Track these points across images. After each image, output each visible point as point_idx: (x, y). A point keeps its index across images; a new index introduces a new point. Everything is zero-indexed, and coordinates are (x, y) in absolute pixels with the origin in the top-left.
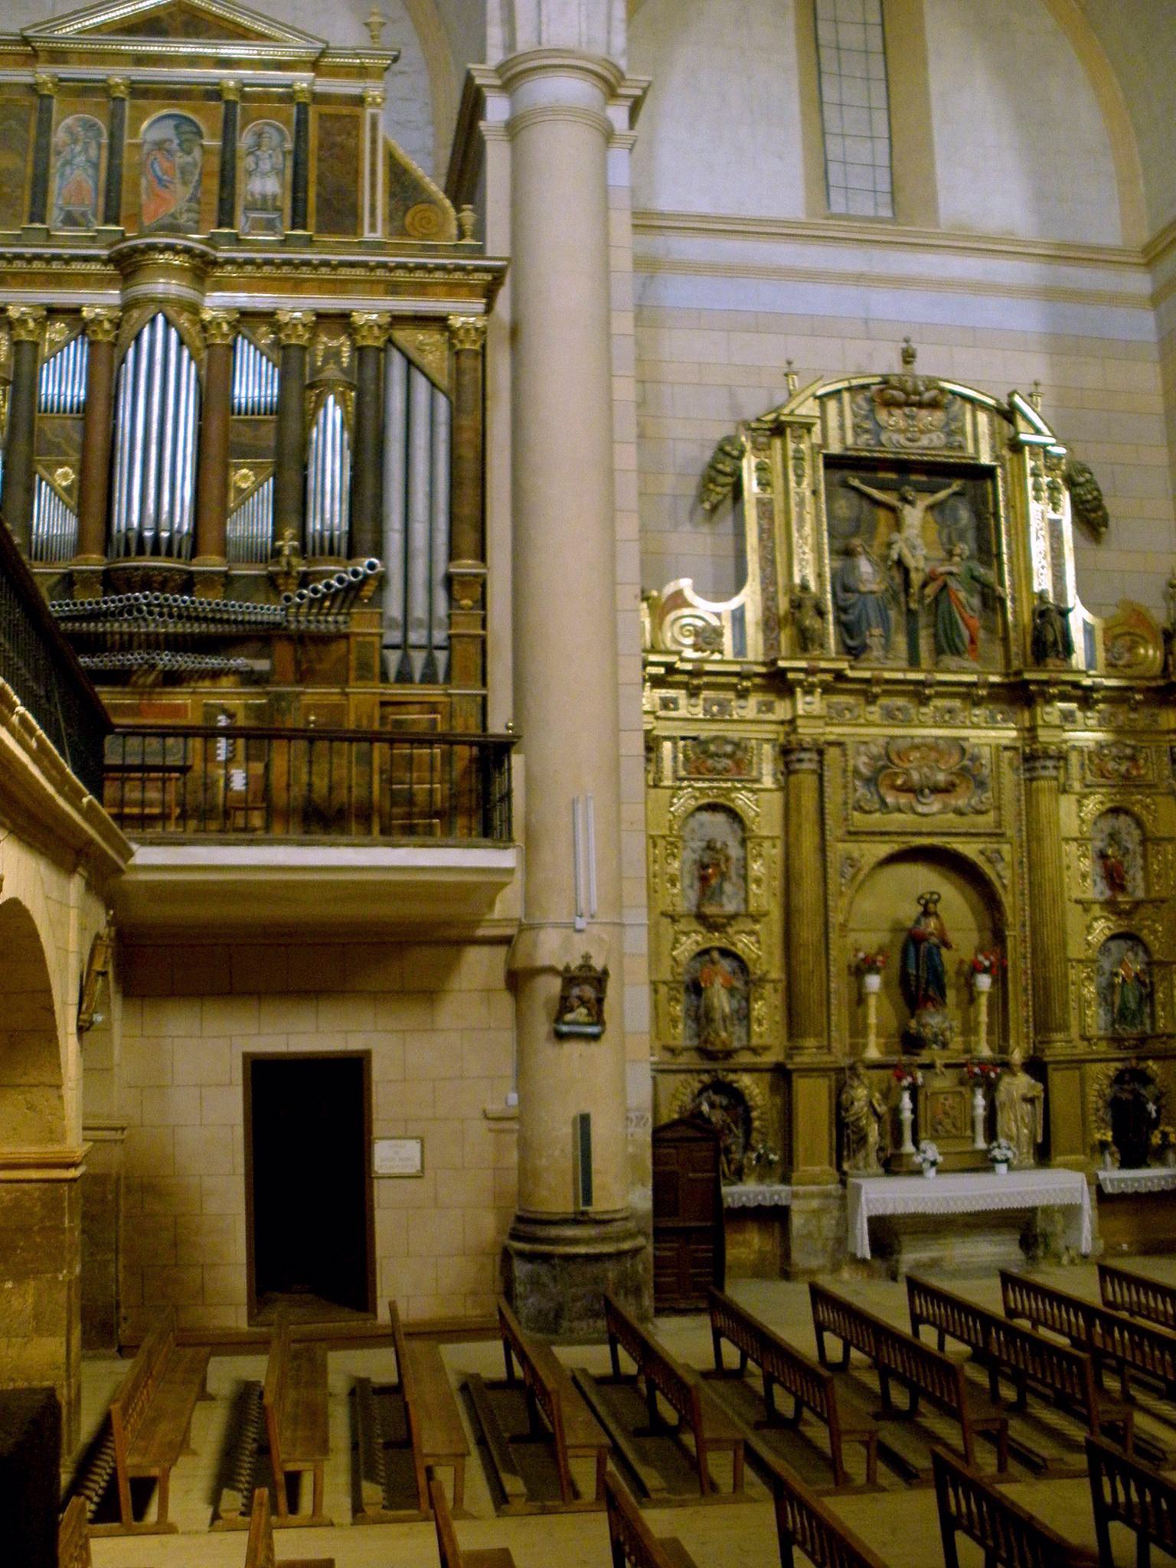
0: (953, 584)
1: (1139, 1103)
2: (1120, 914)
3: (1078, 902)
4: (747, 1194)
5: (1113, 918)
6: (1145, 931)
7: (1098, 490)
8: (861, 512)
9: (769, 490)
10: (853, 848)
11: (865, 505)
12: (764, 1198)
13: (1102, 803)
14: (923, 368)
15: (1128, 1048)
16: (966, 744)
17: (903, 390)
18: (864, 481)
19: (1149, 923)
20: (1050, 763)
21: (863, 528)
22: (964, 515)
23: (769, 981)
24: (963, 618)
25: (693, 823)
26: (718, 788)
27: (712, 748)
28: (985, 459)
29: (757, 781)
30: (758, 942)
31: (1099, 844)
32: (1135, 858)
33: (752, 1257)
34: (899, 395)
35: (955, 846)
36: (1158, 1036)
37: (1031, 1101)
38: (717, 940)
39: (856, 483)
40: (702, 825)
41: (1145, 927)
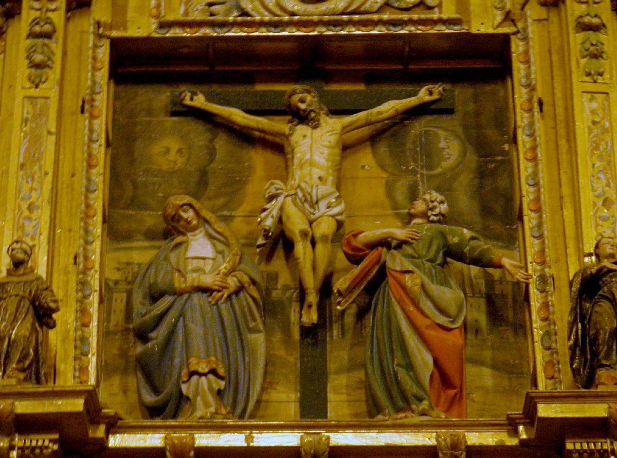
0: (396, 261)
11: (222, 143)
18: (209, 99)
21: (212, 188)
39: (200, 101)
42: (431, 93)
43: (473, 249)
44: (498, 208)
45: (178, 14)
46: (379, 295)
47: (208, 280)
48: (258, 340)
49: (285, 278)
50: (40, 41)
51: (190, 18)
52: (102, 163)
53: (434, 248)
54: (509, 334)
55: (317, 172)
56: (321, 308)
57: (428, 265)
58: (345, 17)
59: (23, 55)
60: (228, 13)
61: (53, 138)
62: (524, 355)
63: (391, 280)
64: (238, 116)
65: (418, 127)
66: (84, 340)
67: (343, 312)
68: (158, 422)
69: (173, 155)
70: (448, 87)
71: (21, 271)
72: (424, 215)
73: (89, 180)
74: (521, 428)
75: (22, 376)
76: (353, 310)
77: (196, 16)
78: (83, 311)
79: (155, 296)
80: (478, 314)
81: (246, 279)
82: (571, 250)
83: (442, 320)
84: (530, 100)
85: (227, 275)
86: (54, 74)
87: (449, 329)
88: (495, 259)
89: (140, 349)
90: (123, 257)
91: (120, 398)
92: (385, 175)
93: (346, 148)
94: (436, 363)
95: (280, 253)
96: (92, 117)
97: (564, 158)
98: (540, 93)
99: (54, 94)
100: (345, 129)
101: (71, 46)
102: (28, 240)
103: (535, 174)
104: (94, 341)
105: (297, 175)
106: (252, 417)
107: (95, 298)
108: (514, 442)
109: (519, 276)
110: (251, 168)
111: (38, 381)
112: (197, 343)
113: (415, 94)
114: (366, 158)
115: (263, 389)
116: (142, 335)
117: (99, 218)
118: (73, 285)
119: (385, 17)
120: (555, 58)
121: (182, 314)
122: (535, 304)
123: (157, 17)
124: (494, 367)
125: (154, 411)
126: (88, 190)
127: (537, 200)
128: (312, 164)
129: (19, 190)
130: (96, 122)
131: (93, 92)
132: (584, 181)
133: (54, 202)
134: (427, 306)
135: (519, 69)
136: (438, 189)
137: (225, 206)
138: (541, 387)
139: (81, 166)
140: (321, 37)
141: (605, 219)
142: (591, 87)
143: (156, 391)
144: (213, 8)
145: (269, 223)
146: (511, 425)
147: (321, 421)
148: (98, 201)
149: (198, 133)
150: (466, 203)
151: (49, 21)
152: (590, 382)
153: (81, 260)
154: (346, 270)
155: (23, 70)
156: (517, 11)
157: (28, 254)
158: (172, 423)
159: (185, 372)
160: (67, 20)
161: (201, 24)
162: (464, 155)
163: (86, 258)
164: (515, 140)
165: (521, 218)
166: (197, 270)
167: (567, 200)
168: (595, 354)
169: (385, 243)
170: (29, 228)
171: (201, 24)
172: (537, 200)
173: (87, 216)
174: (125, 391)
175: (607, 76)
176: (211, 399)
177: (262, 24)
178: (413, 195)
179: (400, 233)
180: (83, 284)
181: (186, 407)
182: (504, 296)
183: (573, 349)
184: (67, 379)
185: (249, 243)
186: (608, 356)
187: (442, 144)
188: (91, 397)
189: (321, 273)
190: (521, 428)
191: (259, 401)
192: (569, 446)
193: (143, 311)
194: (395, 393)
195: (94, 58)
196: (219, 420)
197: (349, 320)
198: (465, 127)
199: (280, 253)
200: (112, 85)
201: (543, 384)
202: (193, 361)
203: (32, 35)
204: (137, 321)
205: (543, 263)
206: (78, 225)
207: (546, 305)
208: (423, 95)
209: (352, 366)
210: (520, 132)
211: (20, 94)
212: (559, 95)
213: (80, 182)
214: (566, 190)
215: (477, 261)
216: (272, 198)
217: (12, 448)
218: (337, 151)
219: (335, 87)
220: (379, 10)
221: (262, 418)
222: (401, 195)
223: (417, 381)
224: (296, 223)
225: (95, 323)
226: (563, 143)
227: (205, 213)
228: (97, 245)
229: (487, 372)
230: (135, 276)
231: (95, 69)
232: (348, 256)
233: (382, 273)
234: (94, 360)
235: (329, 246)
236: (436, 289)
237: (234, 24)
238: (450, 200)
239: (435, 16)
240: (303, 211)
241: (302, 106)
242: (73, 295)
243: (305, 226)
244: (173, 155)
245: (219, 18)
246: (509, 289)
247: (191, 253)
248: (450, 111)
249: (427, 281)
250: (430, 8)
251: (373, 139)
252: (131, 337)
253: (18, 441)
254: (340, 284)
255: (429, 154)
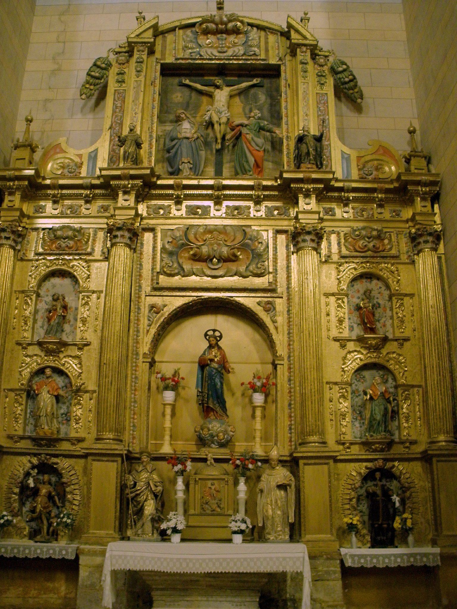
0: (244, 131)
1: (387, 494)
2: (369, 348)
3: (336, 340)
4: (18, 547)
5: (365, 352)
6: (392, 362)
7: (352, 75)
8: (191, 97)
9: (124, 85)
10: (158, 301)
11: (194, 94)
12: (6, 552)
13: (355, 269)
14: (229, 9)
15: (375, 451)
16: (247, 230)
17: (213, 22)
18: (190, 81)
19: (395, 355)
20: (308, 238)
21: (190, 108)
22: (262, 97)
23: (87, 392)
24: (250, 151)
25: (48, 284)
26: (62, 259)
27: (59, 233)
28: (273, 61)
29: (89, 254)
30: (80, 364)
31: (356, 301)
32: (385, 311)
33: (60, 601)
34: (212, 26)
35: (237, 299)
36: (402, 443)
37: (282, 487)
38: (51, 361)
39: (187, 82)
40: (54, 286)
41: (391, 359)
42: (257, 81)
43: (268, 127)
44: (276, 115)
45: (181, 56)
46: (239, 140)
47: (188, 135)
48: (203, 153)
49: (211, 135)
50: (139, 64)
51: (185, 57)
52: (157, 100)
53: (256, 127)
54: (277, 153)
55: (222, 104)
56: (222, 144)
57: (254, 132)
58: (231, 57)
59: (134, 68)
60: (196, 56)
61: (142, 93)
62: (281, 159)
63: (243, 136)
64: (199, 86)
65: (253, 91)
66: (151, 153)
67: (229, 145)
68: (172, 177)
69: (179, 98)
70: (262, 79)
71: (132, 132)
72: (253, 117)
73: (153, 105)
74: (279, 180)
75: (132, 163)
76: (232, 145)
77: (187, 56)
78: (151, 144)
79: (172, 140)
80: (269, 147)
81: (199, 135)
82: (296, 127)
83: (258, 148)
84: (286, 84)
85: (194, 134)
86: (143, 74)
87: (259, 151)
88: (274, 131)
89: (167, 155)
90: (164, 128)
91: (162, 170)
92: (242, 105)
93: (231, 97)
94: (255, 161)
95: (210, 127)
96: (155, 86)
97: (295, 102)
98: (289, 82)
99: (143, 80)
100: (231, 91)
101: (149, 66)
102: (134, 123)
103: (286, 106)
104: (154, 153)
105: (216, 105)
106: (201, 175)
107: (154, 140)
108: (276, 184)
109: (281, 136)
110: (202, 102)
111: (137, 165)
112: (184, 154)
113: (252, 81)
114: (237, 100)
115: (204, 167)
116: (168, 151)
117: (156, 117)
118: (148, 136)
119: (244, 58)
120: (294, 72)
121: (180, 145)
122: (285, 144)
123: (175, 57)
124: (272, 162)
125: (171, 174)
126: (153, 108)
127: (287, 113)
128: (220, 101)
129: (132, 109)
130: (156, 74)
131: (155, 79)
132: (300, 108)
133: (143, 111)
134: (253, 144)
135: (283, 74)
136: (258, 110)
137: (194, 113)
138: (285, 169)
139: (151, 101)
140: (224, 64)
141: (305, 120)
142: (303, 81)
143: (172, 167)
144: (192, 54)
145: (207, 118)
146: (276, 179)
147: (220, 177)
148: (156, 112)
149: (186, 91)
150: (266, 113)
151: (142, 58)
152: (299, 167)
153: (151, 129)
154: (230, 133)
155: (134, 73)
156: (283, 57)
157: (135, 127)
158: (176, 177)
159: (180, 162)
160: (148, 57)
161: (188, 59)
162: (266, 99)
163: (152, 128)
164: (281, 96)
165: (282, 118)
166: (185, 132)
167: (296, 114)
168: (301, 159)
169: (242, 125)
170: (135, 119)
171: (188, 59)
172: (287, 113)
173: (152, 116)
174: (163, 167)
175: (308, 78)
176: (188, 170)
177: (206, 59)
178: (251, 111)
179: (246, 122)
180: (151, 136)
181: (181, 172)
182: (276, 141)
183: (295, 157)
184: (146, 164)
185: (201, 124)
186: (304, 160)
187: (260, 96)
188: (152, 169)
189: (222, 134)
190: (279, 180)
191: (203, 171)
192: (292, 186)
193: (169, 144)
194: (243, 169)
195: (155, 69)
196: (190, 176)
197: (230, 147)
198: (267, 91)
199: (210, 127)
200: (161, 77)
201: (286, 168)
202: (183, 159)
203: (137, 62)
204: (167, 147)
205: (288, 132)
206: (149, 119)
207: (288, 145)
208: (255, 81)
209: (230, 161)
210: (283, 94)
211: (133, 80)
212: (295, 83)
213: (150, 106)
214: (295, 111)
215: (269, 131)
216: (208, 111)
217: (129, 184)
218: (228, 97)
219: (229, 78)
220: (242, 55)
221: (203, 176)
222: (247, 111)
223: (249, 166)
224: (215, 119)
225: (154, 148)
226: (295, 97)
227: (188, 115)
228: (155, 125)
229: (270, 164)
230: (167, 134)
231: (156, 72)
232: (231, 129)
233: (240, 134)
234: (154, 150)
235: (225, 126)
236: (256, 139)
237: (198, 59)
238: (262, 113)
239: (259, 58)
240: (217, 115)
241: (218, 84)
242: (148, 139)
243: (218, 120)
244: (179, 98)
245: (194, 57)
246: (278, 140)
247: (183, 127)
248: (262, 86)
249: (253, 137)
250: (257, 56)
251: (239, 94)
252: (165, 152)
253: (131, 182)
254: (228, 137)
255: (256, 99)
